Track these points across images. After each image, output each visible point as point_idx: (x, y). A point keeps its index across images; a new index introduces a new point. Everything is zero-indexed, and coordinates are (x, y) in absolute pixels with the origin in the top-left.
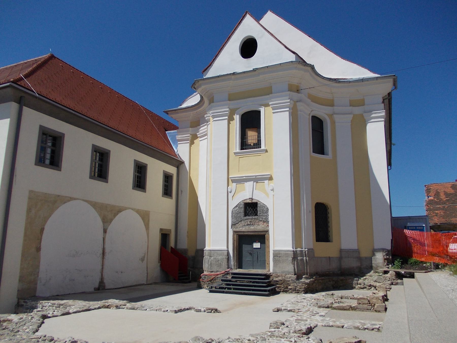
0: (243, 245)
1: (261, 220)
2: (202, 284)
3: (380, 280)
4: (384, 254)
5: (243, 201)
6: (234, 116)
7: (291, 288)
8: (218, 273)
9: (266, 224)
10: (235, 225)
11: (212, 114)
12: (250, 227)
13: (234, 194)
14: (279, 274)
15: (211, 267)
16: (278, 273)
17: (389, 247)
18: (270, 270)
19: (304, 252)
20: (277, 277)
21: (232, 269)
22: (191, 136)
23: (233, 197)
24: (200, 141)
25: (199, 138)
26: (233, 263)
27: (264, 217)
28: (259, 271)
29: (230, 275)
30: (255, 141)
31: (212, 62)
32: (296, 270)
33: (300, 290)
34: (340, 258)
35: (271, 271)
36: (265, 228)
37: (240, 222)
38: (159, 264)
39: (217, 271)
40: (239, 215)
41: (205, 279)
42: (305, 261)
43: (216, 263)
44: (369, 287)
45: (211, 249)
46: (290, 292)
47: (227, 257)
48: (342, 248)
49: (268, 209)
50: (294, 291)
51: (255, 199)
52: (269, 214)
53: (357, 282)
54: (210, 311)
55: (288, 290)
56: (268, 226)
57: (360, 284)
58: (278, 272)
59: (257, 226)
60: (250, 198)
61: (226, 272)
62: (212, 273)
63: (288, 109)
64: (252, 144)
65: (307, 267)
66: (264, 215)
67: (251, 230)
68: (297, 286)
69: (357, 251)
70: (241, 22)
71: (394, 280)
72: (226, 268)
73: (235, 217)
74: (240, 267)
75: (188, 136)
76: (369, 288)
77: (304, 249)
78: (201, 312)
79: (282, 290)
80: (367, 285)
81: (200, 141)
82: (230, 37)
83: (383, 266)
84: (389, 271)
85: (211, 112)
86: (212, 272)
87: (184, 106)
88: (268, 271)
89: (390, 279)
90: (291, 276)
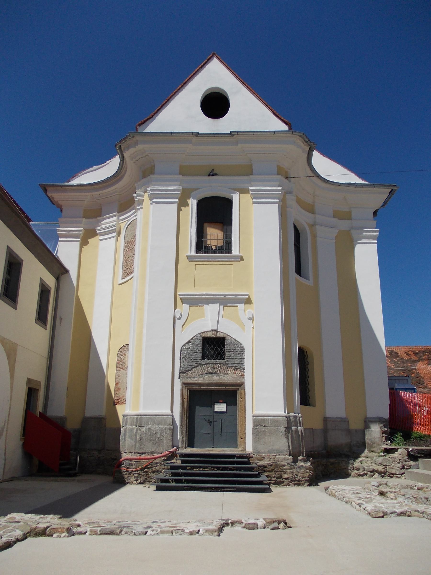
0: (197, 408)
1: (231, 367)
2: (126, 476)
3: (387, 462)
4: (382, 425)
5: (201, 334)
6: (188, 201)
7: (288, 477)
8: (156, 455)
9: (239, 372)
10: (185, 373)
11: (151, 192)
12: (212, 376)
13: (186, 321)
14: (264, 455)
15: (140, 446)
16: (262, 453)
17: (386, 415)
18: (245, 449)
19: (299, 418)
20: (261, 460)
21: (178, 447)
22: (83, 231)
23: (183, 326)
24: (101, 240)
25: (99, 236)
26: (181, 438)
27: (236, 362)
28: (227, 451)
29: (177, 457)
30: (220, 243)
31: (155, 114)
32: (291, 448)
33: (303, 479)
34: (325, 431)
35: (249, 448)
36: (238, 378)
37: (194, 368)
38: (21, 443)
39: (153, 452)
40: (193, 357)
41: (131, 467)
42: (300, 434)
43: (151, 438)
44: (371, 473)
45: (142, 414)
46: (286, 484)
47: (172, 427)
48: (328, 415)
49: (242, 349)
50: (293, 482)
51: (222, 332)
52: (245, 357)
53: (353, 466)
54: (276, 525)
55: (283, 480)
56: (243, 376)
57: (358, 469)
58: (263, 451)
59: (223, 376)
60: (213, 330)
61: (171, 452)
62: (143, 456)
63: (278, 200)
64: (214, 248)
65: (302, 442)
66: (236, 357)
67: (214, 382)
68: (297, 474)
69: (345, 421)
70: (205, 66)
71: (406, 462)
72: (170, 447)
73: (185, 359)
74: (191, 444)
75: (80, 231)
76: (371, 475)
77: (297, 415)
78: (257, 528)
79: (272, 482)
80: (369, 470)
81: (101, 240)
82: (186, 83)
83: (380, 443)
84: (398, 449)
85: (151, 187)
86: (143, 453)
87: (76, 181)
88: (242, 451)
89: (401, 460)
90: (285, 458)
